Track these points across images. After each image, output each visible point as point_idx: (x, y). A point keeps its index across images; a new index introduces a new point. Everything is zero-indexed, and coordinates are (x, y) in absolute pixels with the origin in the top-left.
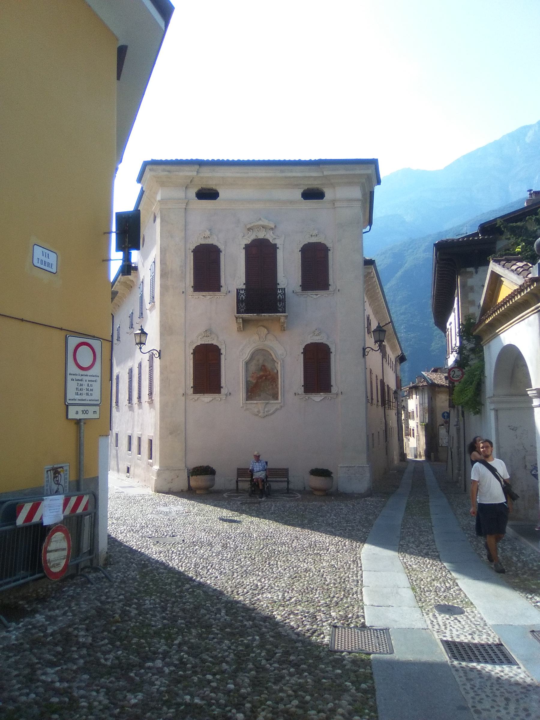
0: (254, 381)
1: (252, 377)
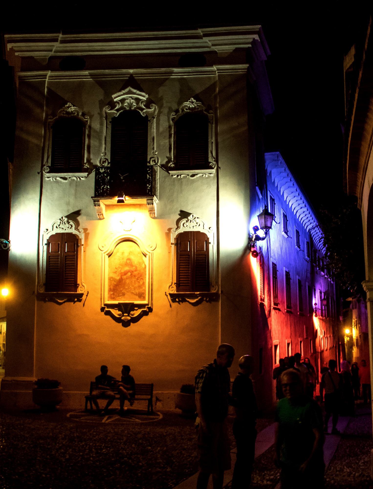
0: (118, 278)
1: (115, 272)
